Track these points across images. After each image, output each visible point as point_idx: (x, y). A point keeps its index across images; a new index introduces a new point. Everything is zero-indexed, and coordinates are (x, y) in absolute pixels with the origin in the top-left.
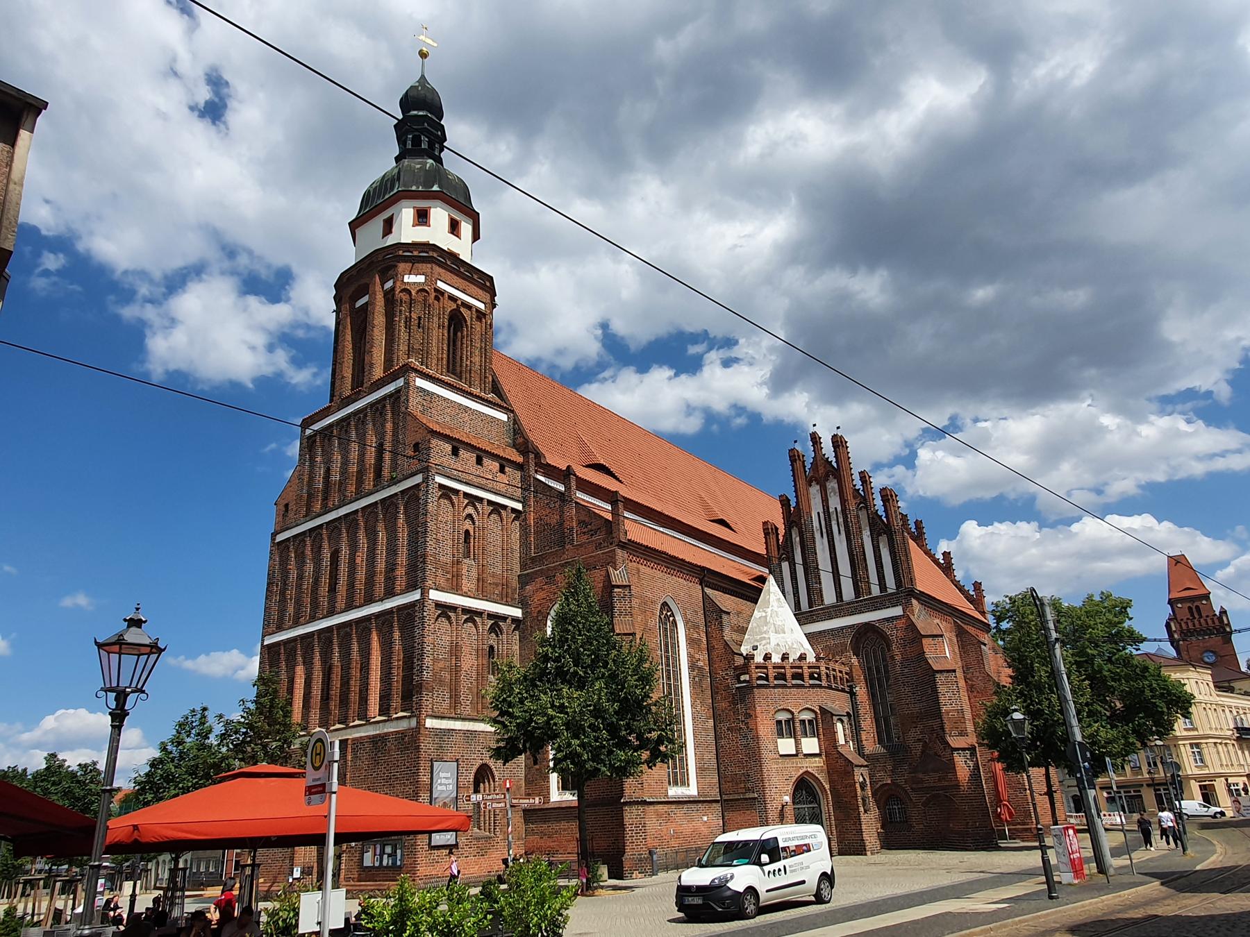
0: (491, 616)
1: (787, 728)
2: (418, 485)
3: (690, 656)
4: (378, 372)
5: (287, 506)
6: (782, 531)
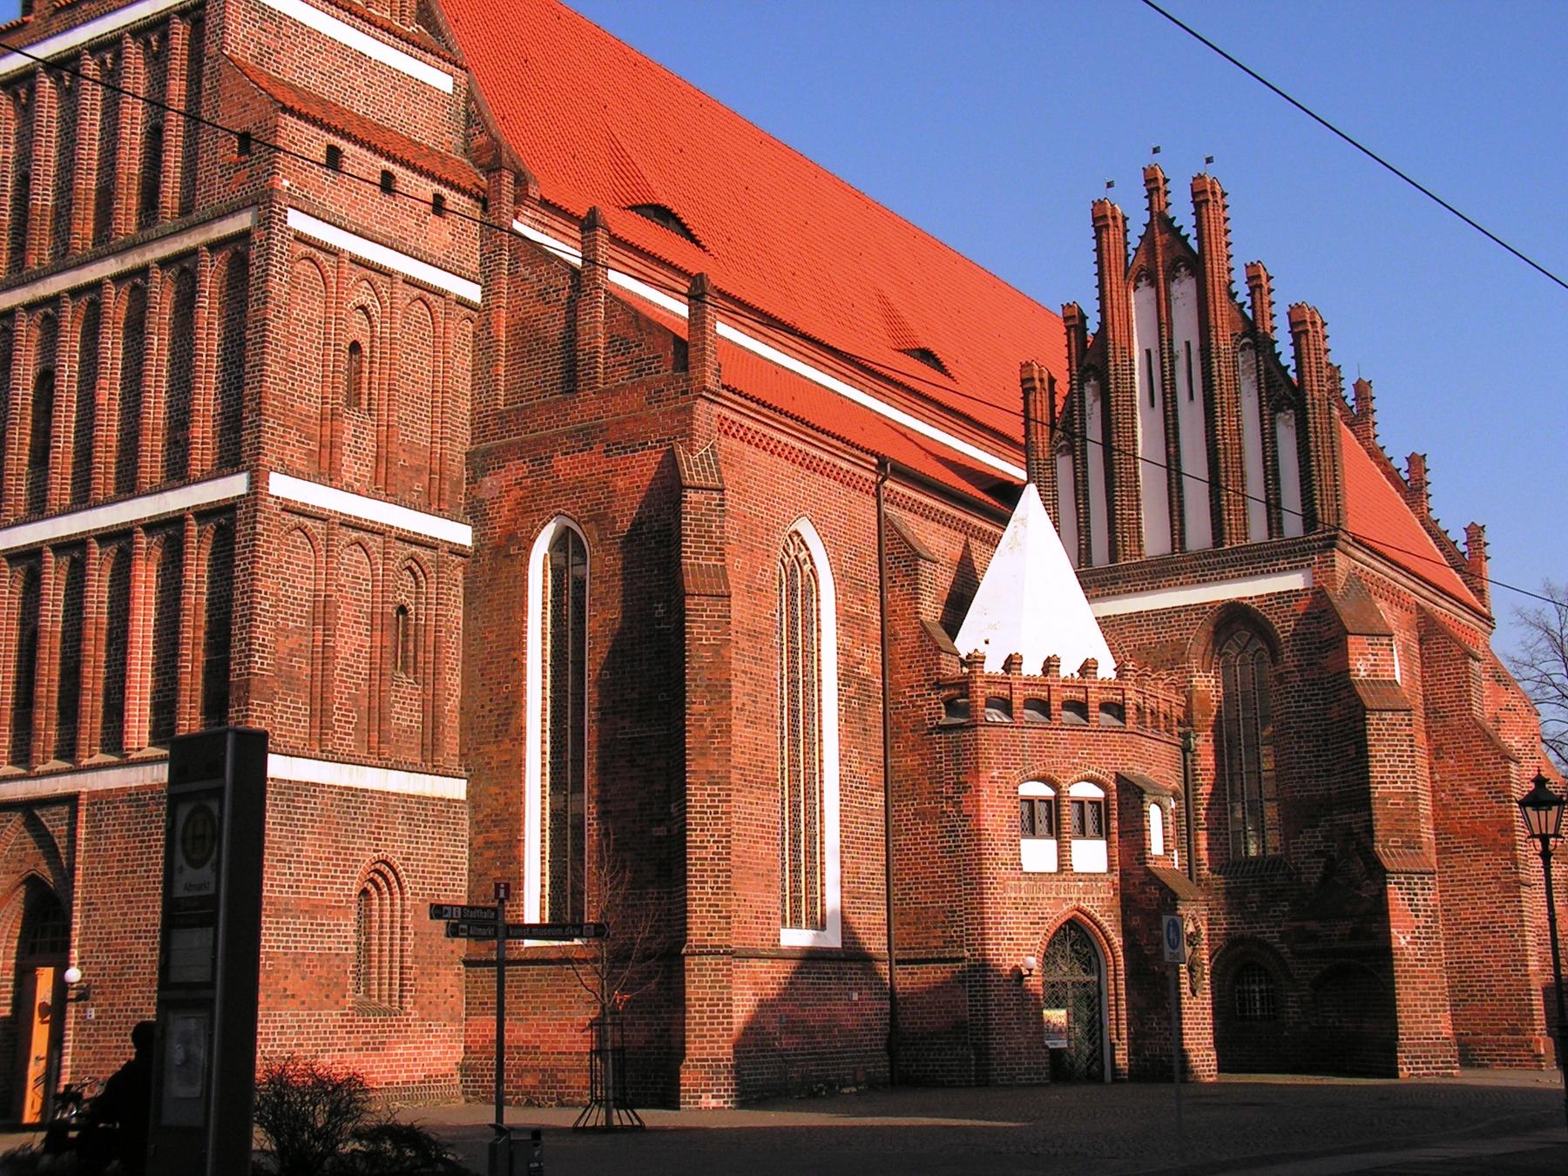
1: (1048, 819)
3: (843, 652)
6: (1062, 387)
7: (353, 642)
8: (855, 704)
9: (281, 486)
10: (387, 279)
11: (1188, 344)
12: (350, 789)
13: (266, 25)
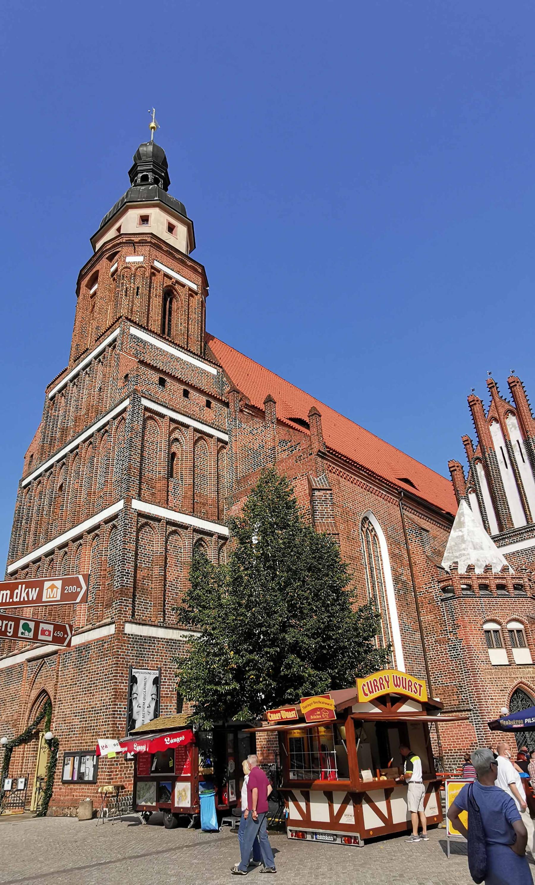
0: (197, 531)
1: (492, 639)
2: (124, 410)
3: (393, 569)
6: (466, 469)
8: (401, 592)
11: (518, 441)
12: (173, 640)
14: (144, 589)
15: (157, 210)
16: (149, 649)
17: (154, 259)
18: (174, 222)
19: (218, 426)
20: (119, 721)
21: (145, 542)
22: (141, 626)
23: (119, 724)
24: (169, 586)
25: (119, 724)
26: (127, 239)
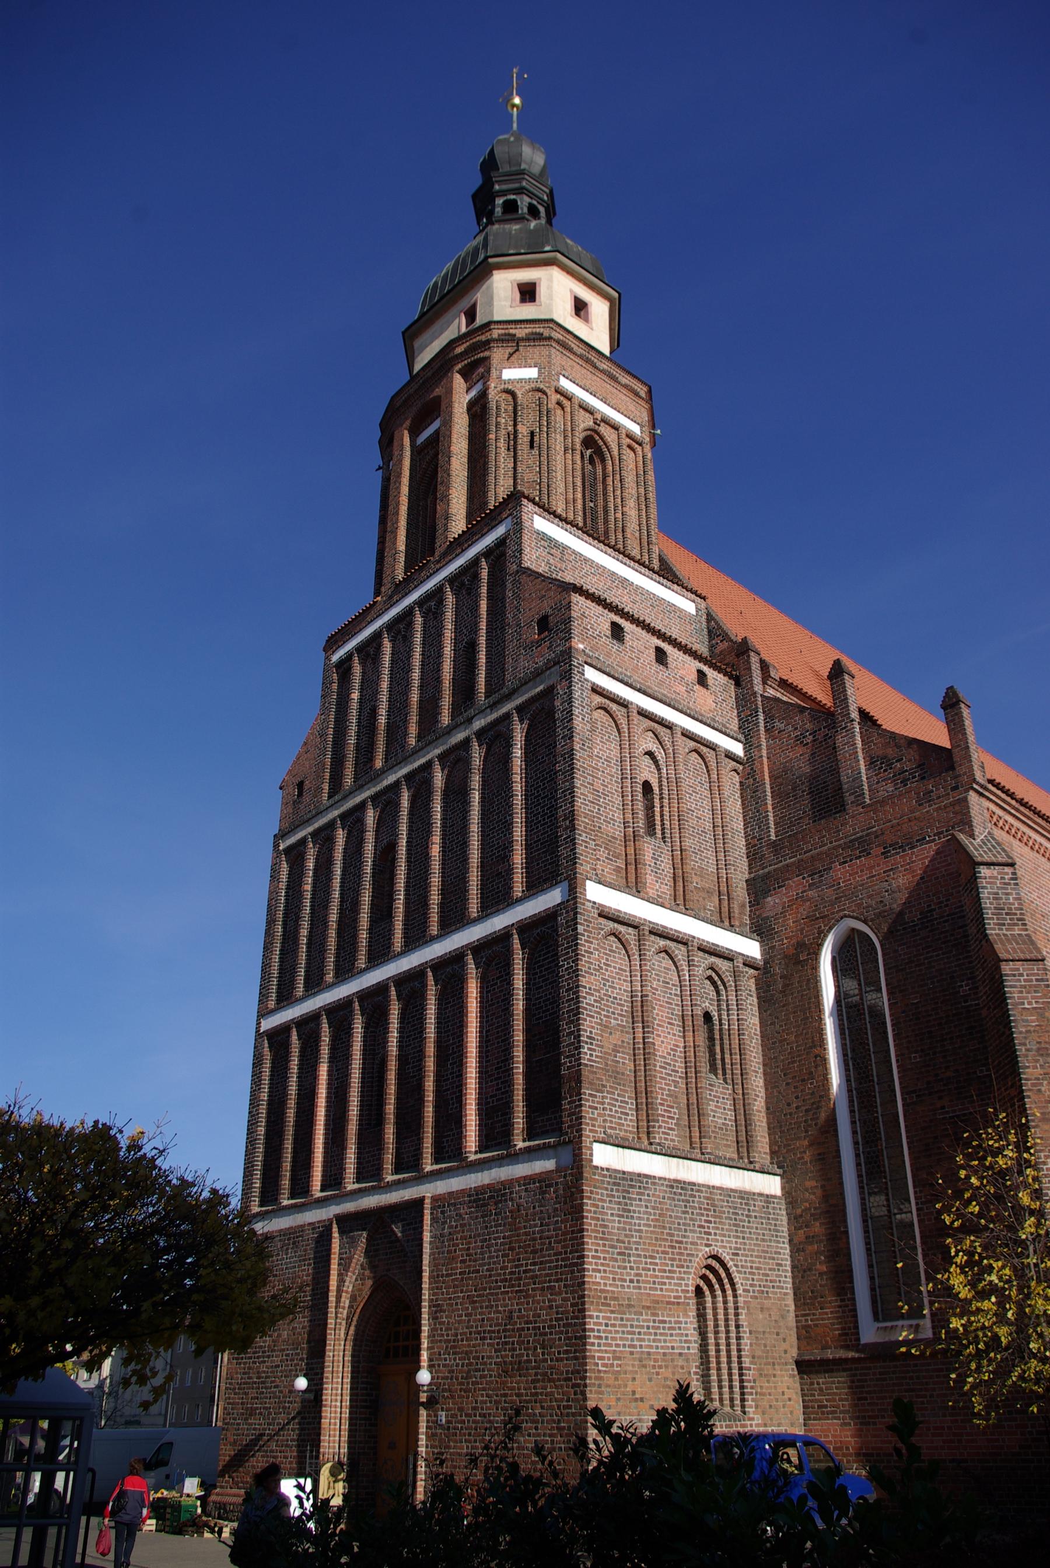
4: (458, 525)
5: (300, 785)
7: (668, 1041)
9: (595, 893)
10: (668, 731)
13: (553, 551)
14: (618, 1073)
15: (555, 273)
16: (640, 1200)
17: (559, 374)
18: (586, 294)
19: (724, 725)
20: (598, 1351)
21: (612, 972)
22: (620, 1149)
23: (600, 1358)
24: (661, 1067)
25: (600, 1358)
26: (500, 332)
